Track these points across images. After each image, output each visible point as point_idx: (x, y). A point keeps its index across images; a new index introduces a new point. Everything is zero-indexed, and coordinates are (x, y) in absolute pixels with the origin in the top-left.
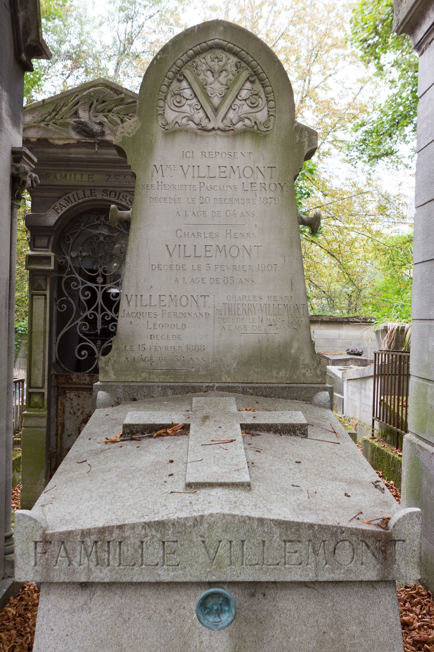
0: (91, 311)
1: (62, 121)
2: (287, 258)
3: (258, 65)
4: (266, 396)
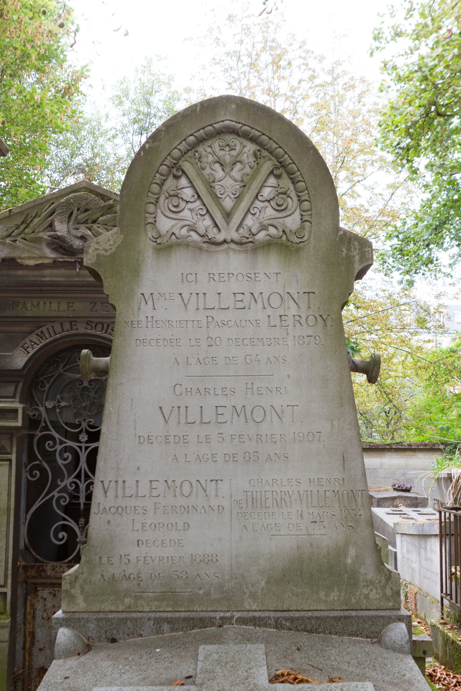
0: (71, 479)
1: (33, 235)
2: (335, 423)
3: (286, 153)
4: (310, 631)
